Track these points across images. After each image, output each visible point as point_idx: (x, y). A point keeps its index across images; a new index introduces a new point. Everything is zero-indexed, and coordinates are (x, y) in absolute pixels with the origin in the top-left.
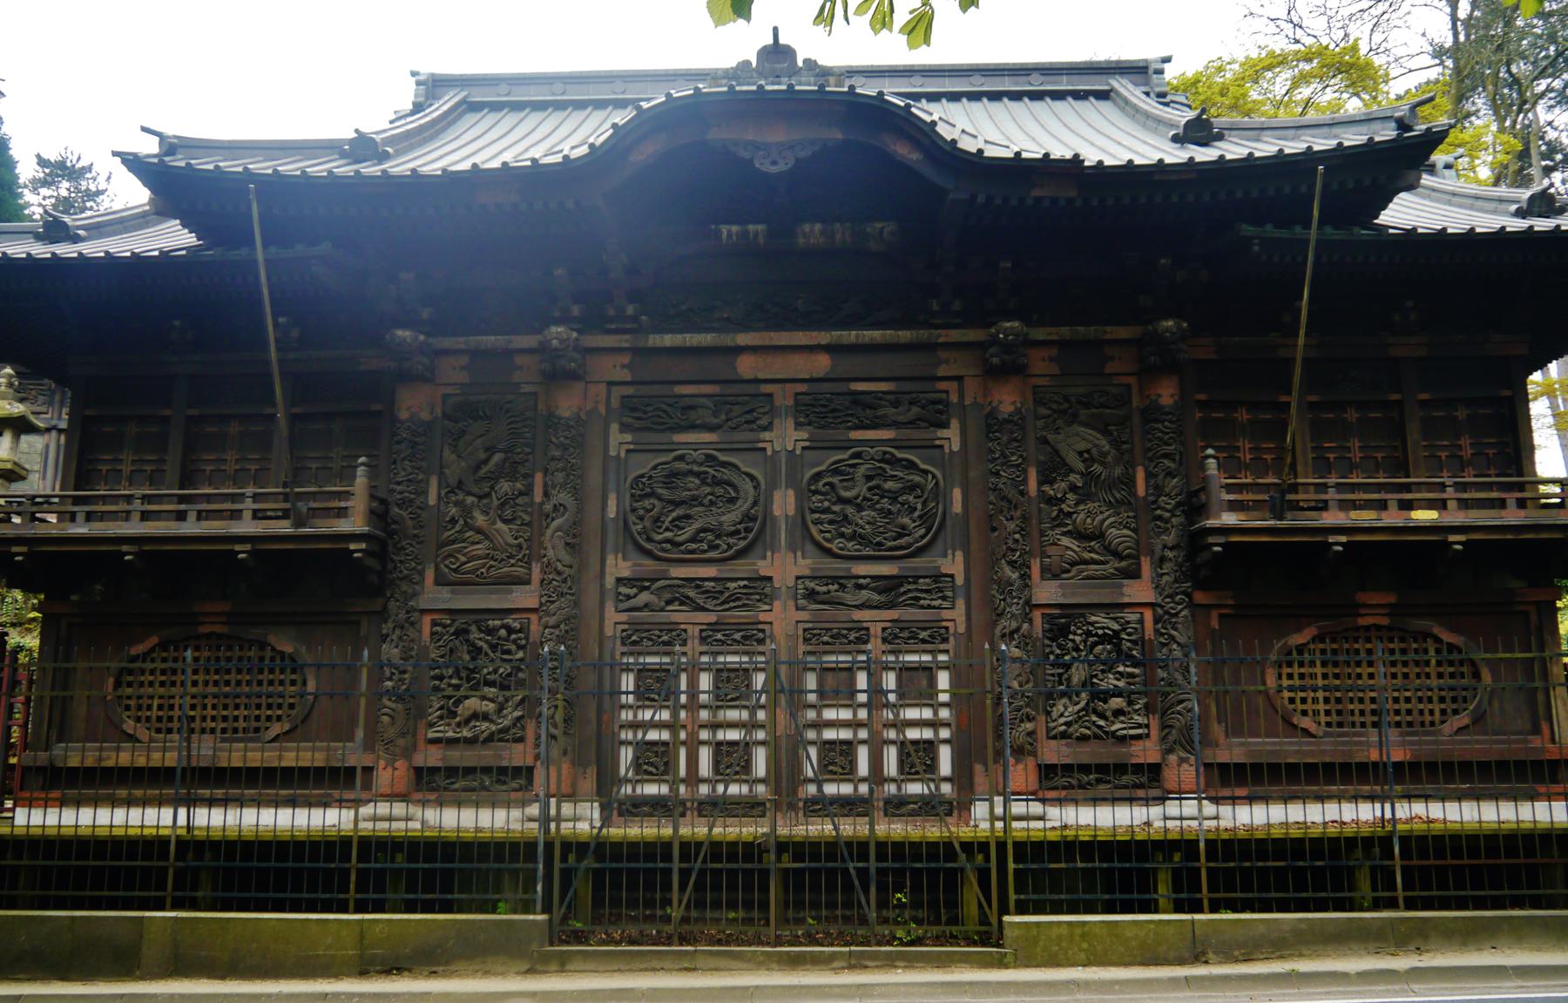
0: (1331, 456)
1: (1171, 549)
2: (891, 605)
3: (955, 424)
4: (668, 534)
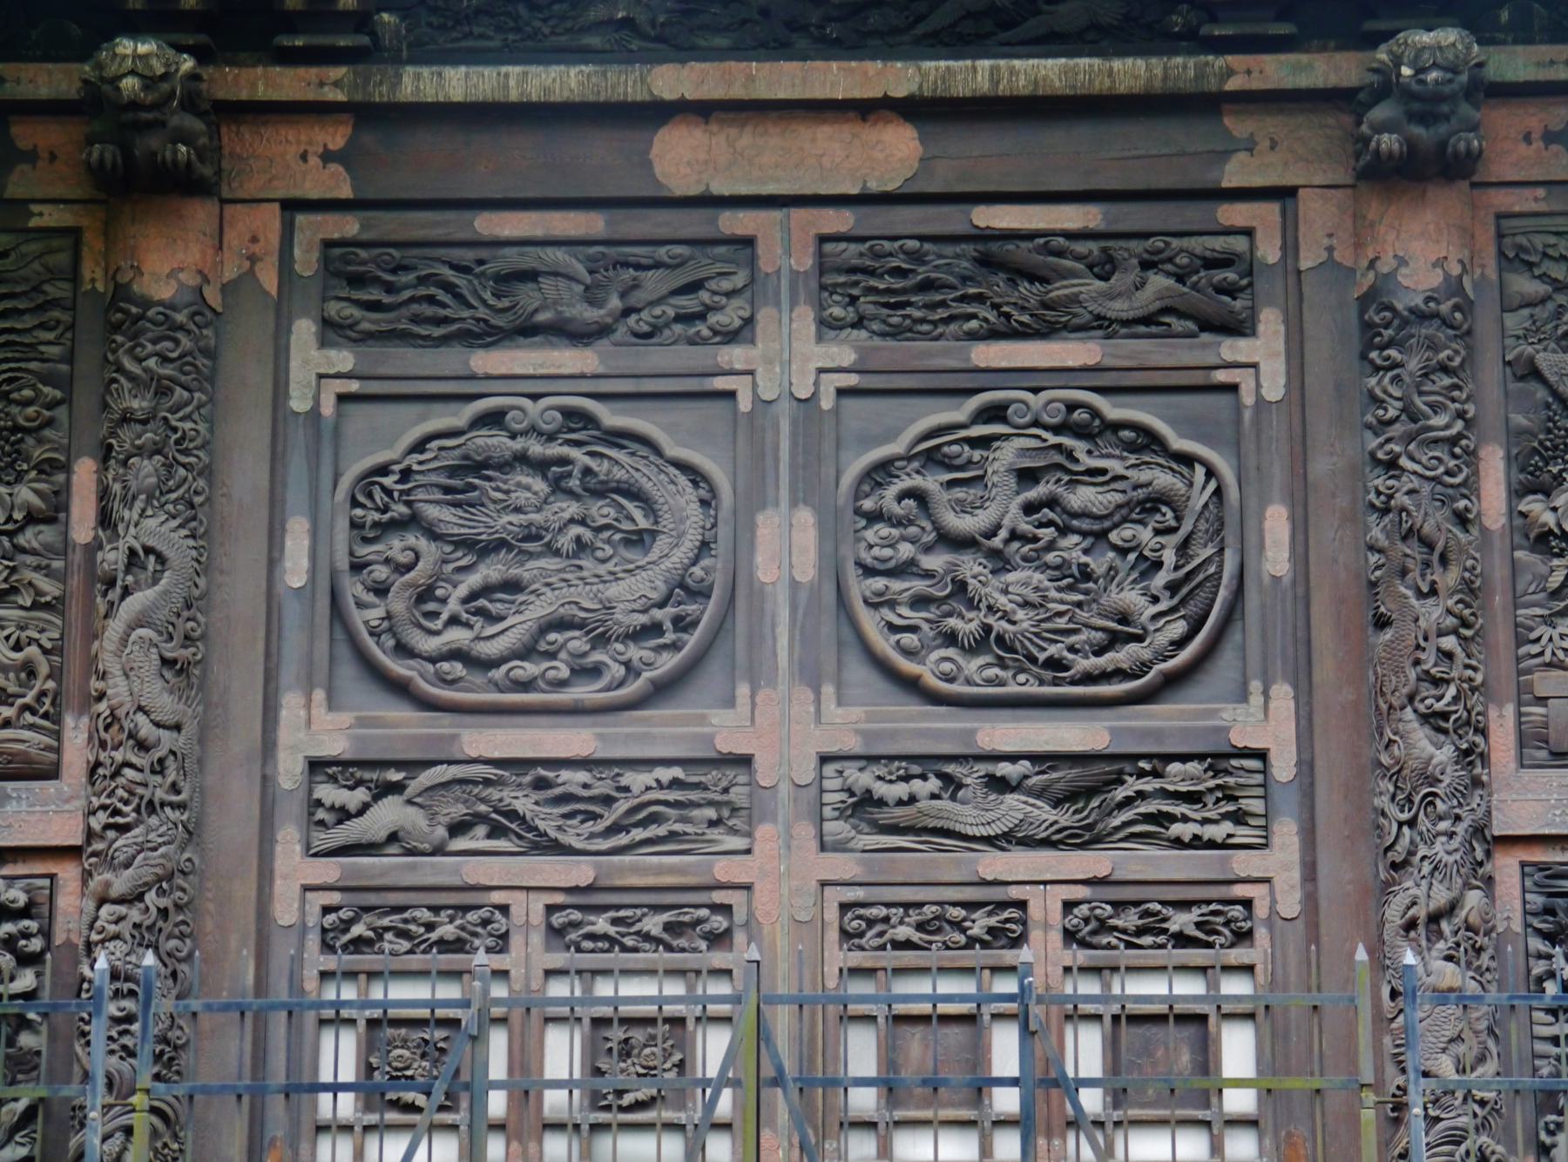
2: (1087, 838)
3: (1270, 322)
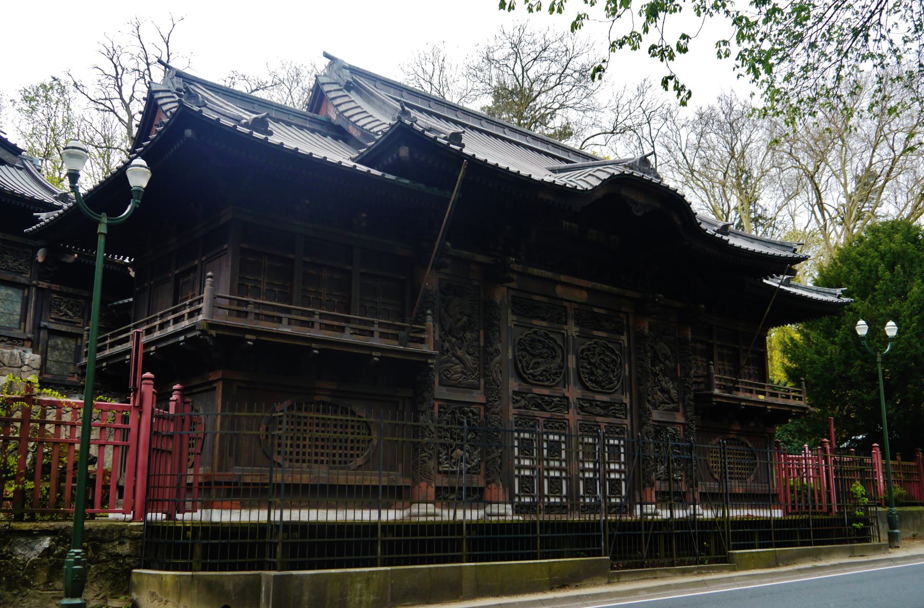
3: (625, 334)
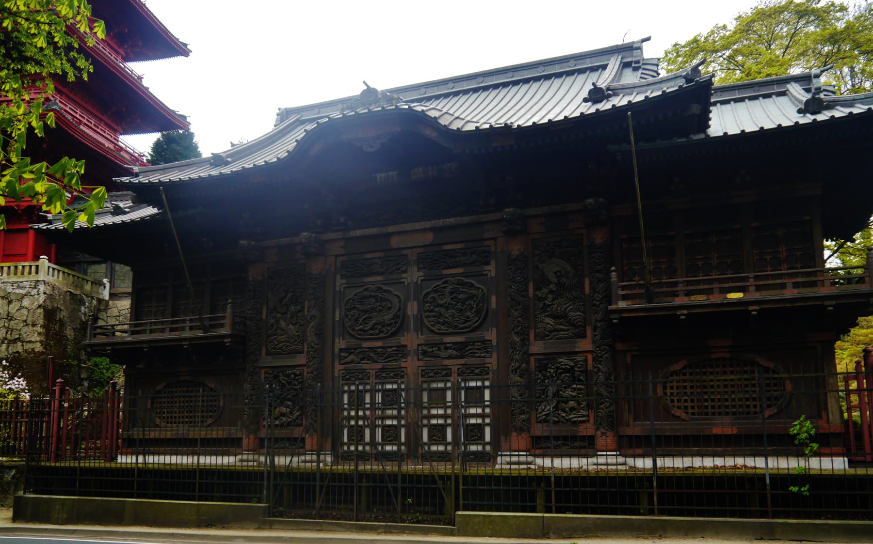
0: (700, 263)
1: (600, 321)
2: (462, 357)
3: (493, 262)
4: (361, 327)
